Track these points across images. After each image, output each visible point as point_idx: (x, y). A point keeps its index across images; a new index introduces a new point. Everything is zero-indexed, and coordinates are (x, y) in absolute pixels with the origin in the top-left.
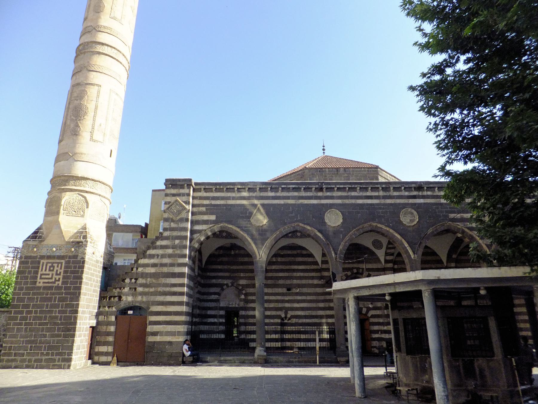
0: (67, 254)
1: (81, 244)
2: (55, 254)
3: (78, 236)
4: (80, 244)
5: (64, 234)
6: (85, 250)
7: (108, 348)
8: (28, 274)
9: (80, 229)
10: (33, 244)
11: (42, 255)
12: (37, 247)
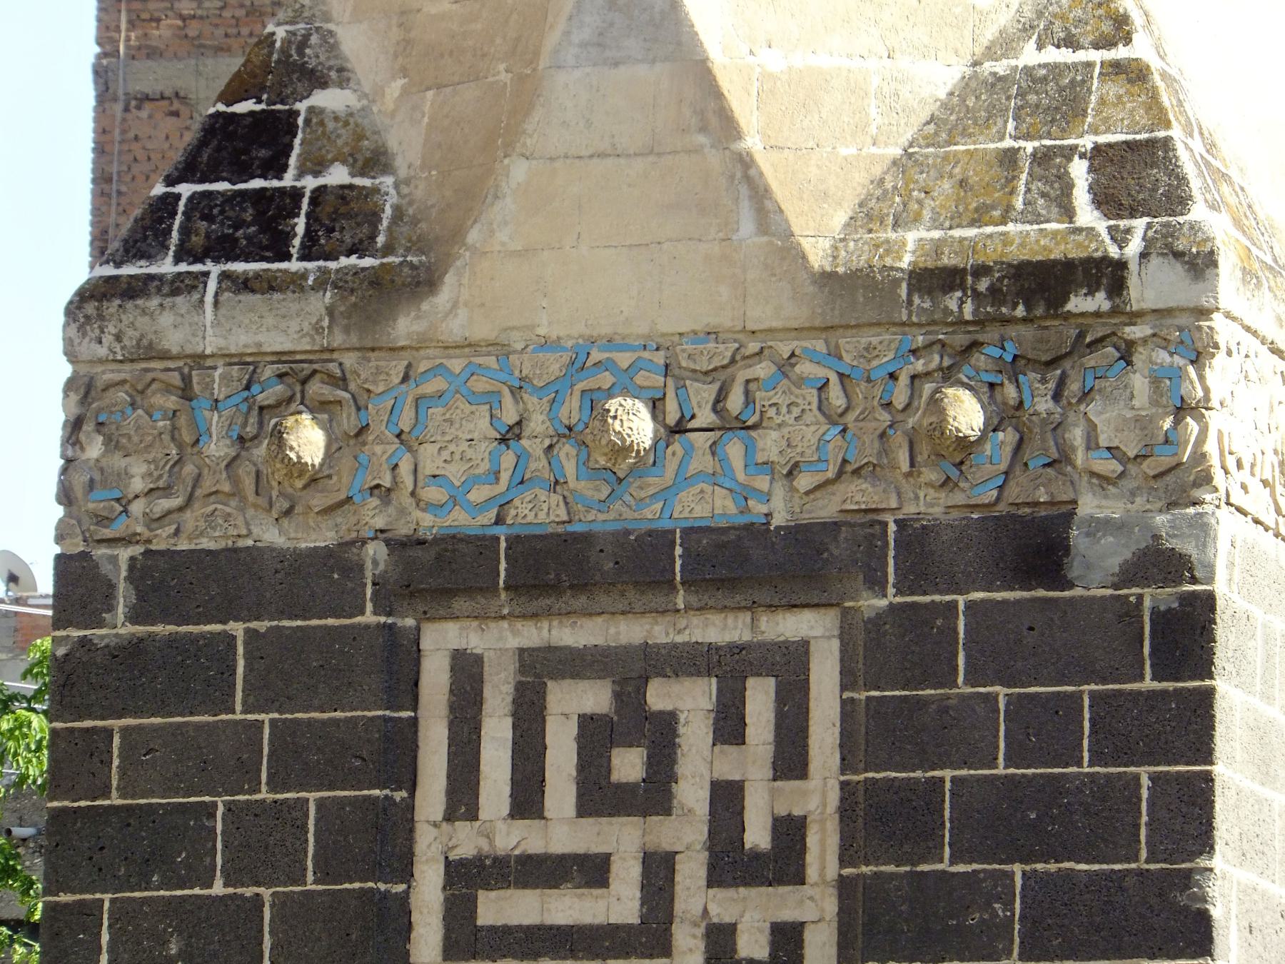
0: (858, 494)
1: (1100, 301)
2: (651, 515)
3: (1009, 158)
4: (1079, 303)
5: (752, 142)
6: (1183, 409)
7: (770, 744)
8: (257, 900)
9: (1005, 45)
10: (240, 341)
11: (428, 523)
12: (316, 388)
